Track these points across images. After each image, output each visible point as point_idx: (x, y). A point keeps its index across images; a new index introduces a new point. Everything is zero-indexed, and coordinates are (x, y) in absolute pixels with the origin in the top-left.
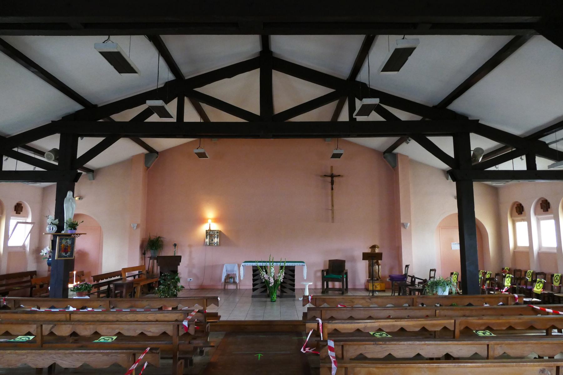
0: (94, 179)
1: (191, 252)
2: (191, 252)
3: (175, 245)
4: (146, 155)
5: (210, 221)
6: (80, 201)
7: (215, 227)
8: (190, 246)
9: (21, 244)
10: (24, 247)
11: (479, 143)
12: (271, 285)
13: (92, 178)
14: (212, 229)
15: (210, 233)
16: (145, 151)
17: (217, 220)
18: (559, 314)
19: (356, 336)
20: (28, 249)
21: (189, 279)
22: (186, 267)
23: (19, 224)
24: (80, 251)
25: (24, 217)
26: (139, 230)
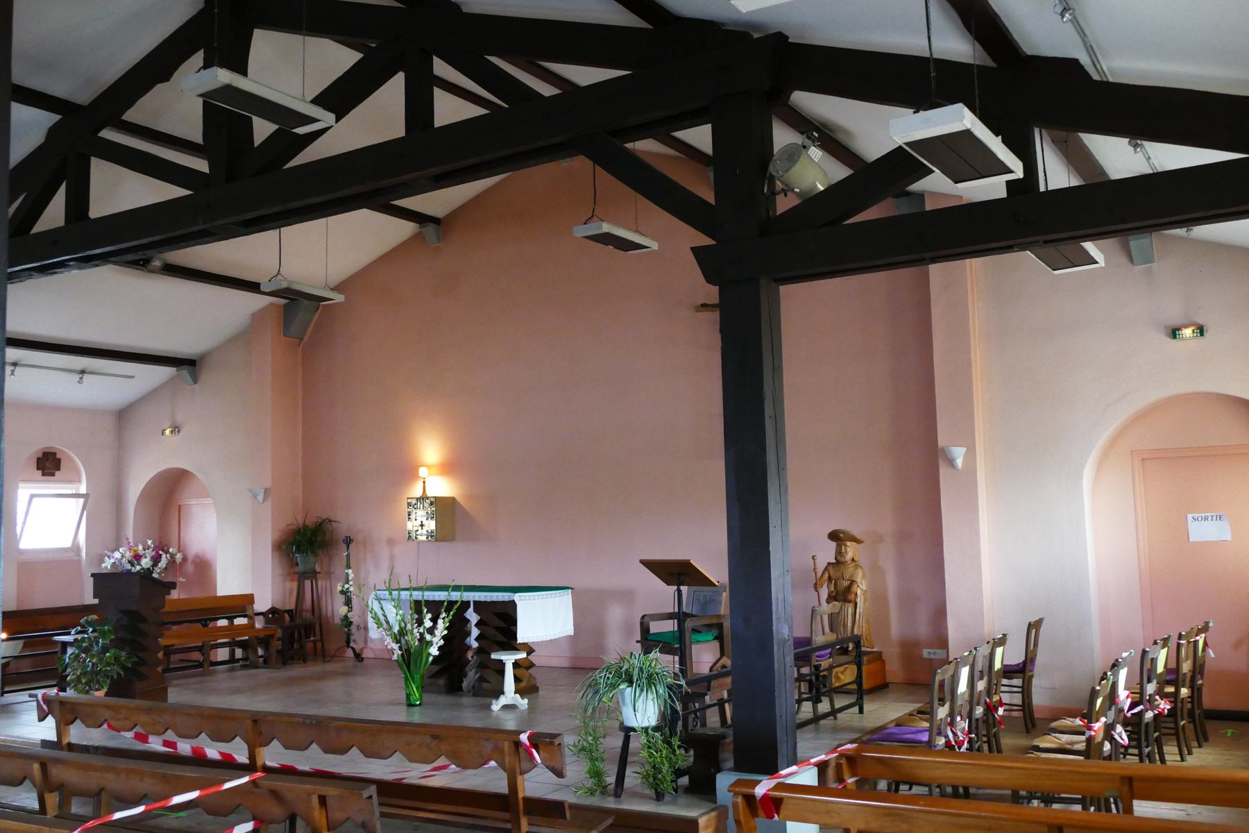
1: (392, 557)
2: (392, 557)
3: (348, 541)
4: (285, 305)
5: (423, 472)
6: (176, 438)
7: (441, 487)
8: (391, 542)
10: (75, 548)
12: (395, 657)
15: (443, 508)
20: (84, 554)
24: (197, 556)
25: (70, 482)
26: (269, 503)
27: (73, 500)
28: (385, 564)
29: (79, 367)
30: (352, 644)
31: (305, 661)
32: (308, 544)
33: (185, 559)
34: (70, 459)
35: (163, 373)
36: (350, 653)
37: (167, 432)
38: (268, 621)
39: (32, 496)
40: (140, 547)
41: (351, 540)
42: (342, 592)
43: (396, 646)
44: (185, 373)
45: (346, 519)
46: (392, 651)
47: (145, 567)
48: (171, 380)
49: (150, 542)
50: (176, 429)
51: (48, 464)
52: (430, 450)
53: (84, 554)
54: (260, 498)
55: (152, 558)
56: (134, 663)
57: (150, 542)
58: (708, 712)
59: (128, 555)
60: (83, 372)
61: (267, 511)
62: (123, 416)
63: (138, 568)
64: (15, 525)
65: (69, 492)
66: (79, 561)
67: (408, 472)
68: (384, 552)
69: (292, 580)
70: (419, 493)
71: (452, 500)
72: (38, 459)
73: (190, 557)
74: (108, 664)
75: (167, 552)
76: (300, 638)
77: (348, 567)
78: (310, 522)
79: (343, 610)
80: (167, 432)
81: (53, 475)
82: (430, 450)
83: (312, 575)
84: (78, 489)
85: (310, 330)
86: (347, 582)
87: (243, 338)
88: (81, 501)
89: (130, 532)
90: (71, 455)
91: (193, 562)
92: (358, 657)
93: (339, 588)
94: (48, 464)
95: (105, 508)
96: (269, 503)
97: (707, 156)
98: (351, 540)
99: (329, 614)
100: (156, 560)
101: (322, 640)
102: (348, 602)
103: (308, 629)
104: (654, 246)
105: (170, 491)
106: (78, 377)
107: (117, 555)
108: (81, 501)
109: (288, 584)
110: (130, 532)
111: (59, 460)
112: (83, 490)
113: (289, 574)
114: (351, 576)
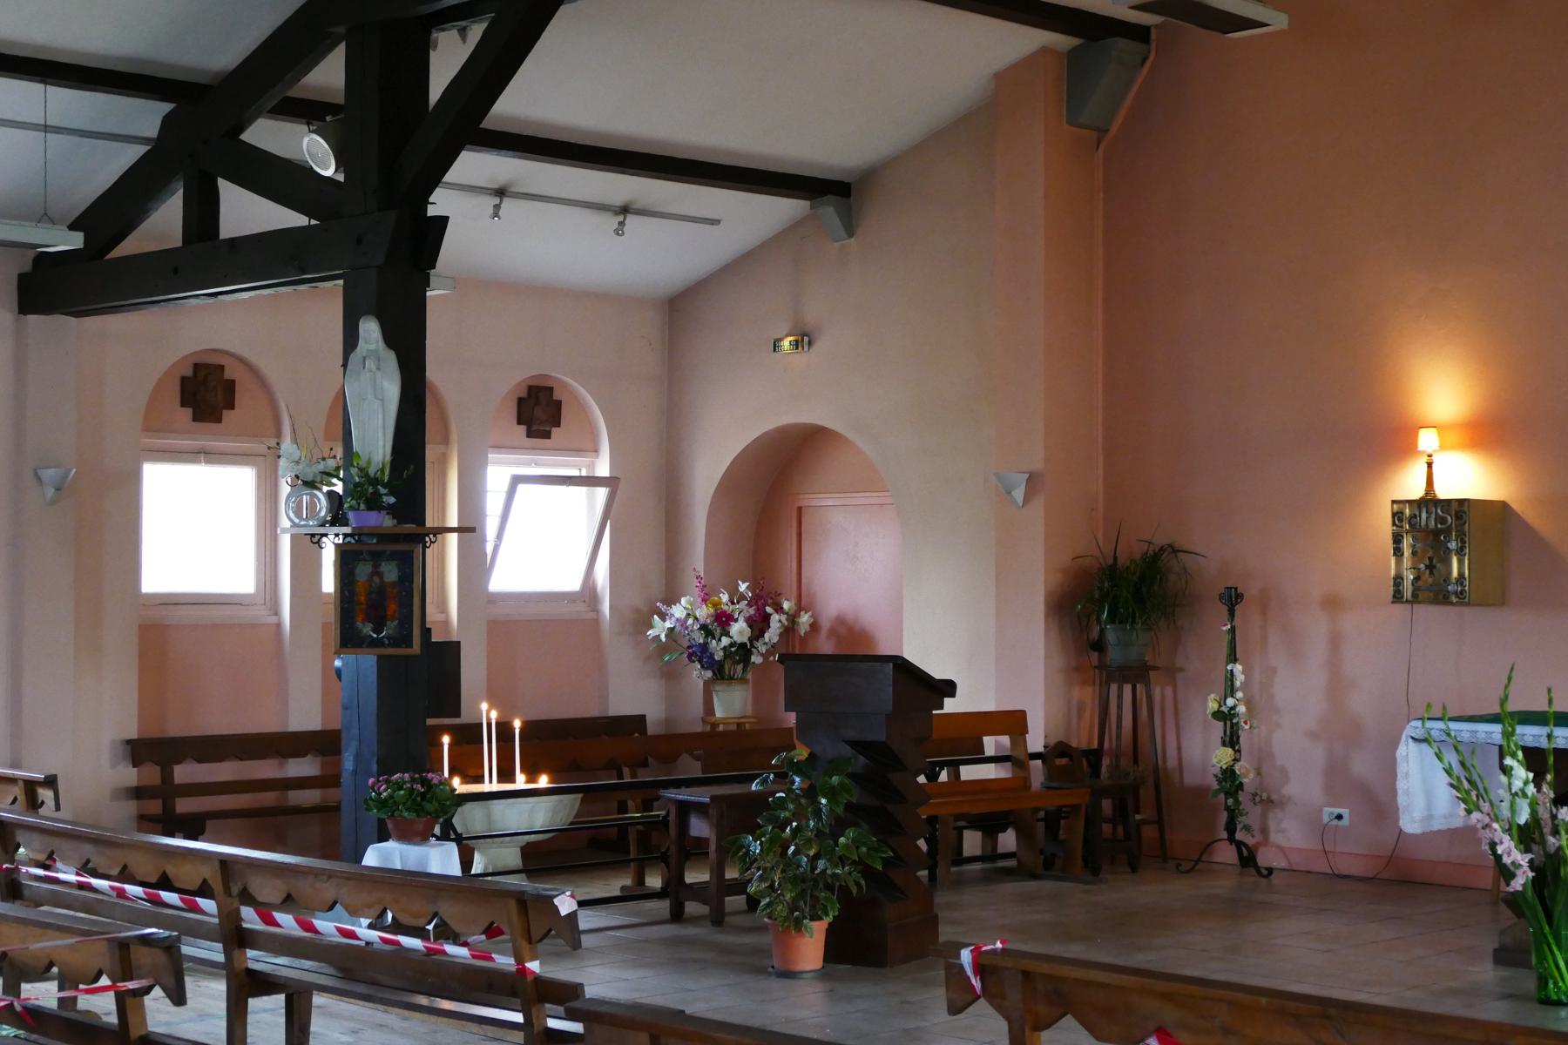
0: (851, 234)
1: (1336, 642)
2: (1336, 642)
3: (1232, 599)
4: (1073, 53)
5: (1427, 440)
6: (803, 358)
7: (1465, 476)
8: (1332, 604)
9: (573, 584)
10: (588, 593)
11: (245, 212)
12: (1518, 884)
13: (843, 233)
14: (1443, 492)
15: (1437, 525)
16: (1062, 41)
17: (1485, 433)
18: (492, 959)
19: (66, 946)
20: (606, 607)
21: (1328, 812)
22: (1313, 736)
23: (521, 488)
24: (840, 620)
25: (578, 451)
26: (1039, 504)
27: (581, 491)
28: (1317, 651)
29: (618, 201)
30: (1239, 836)
31: (1134, 869)
32: (1124, 603)
33: (814, 626)
34: (582, 407)
35: (778, 210)
36: (1226, 854)
37: (786, 343)
38: (1051, 773)
39: (517, 480)
40: (725, 598)
41: (1239, 597)
42: (1218, 715)
43: (1523, 859)
44: (829, 211)
45: (1217, 546)
46: (1507, 873)
47: (738, 639)
48: (792, 230)
49: (743, 587)
50: (804, 339)
51: (539, 413)
52: (1441, 391)
53: (606, 607)
54: (1018, 495)
55: (750, 621)
56: (886, 862)
57: (743, 587)
58: (452, 849)
59: (704, 612)
60: (625, 210)
61: (1035, 519)
62: (680, 311)
63: (725, 641)
64: (483, 540)
65: (574, 472)
66: (596, 622)
67: (1394, 439)
68: (1316, 627)
69: (1084, 683)
70: (1416, 491)
71: (1503, 506)
72: (520, 401)
73: (825, 624)
74: (842, 861)
75: (779, 609)
76: (1113, 812)
77: (1233, 658)
78: (1131, 551)
79: (1223, 756)
80: (786, 343)
81: (547, 435)
82: (1441, 391)
83: (1138, 673)
84: (592, 466)
85: (1123, 112)
86: (1231, 690)
87: (976, 127)
88: (602, 493)
89: (697, 557)
90: (586, 399)
91: (833, 632)
92: (1248, 859)
93: (1212, 706)
94: (539, 412)
95: (645, 514)
96: (1039, 504)
97: (242, 130)
98: (1239, 597)
99: (1172, 762)
100: (759, 624)
101: (1160, 822)
102: (1232, 740)
103: (1126, 796)
104: (1278, 21)
105: (780, 476)
106: (614, 221)
107: (678, 611)
108: (602, 493)
109: (1076, 692)
110: (697, 557)
111: (559, 404)
112: (603, 469)
113: (1078, 669)
114: (1240, 679)
